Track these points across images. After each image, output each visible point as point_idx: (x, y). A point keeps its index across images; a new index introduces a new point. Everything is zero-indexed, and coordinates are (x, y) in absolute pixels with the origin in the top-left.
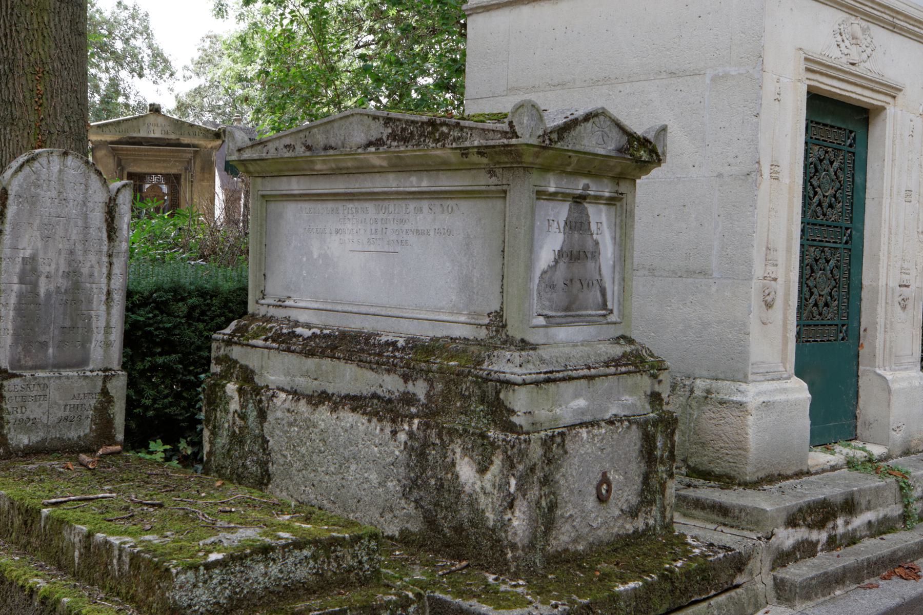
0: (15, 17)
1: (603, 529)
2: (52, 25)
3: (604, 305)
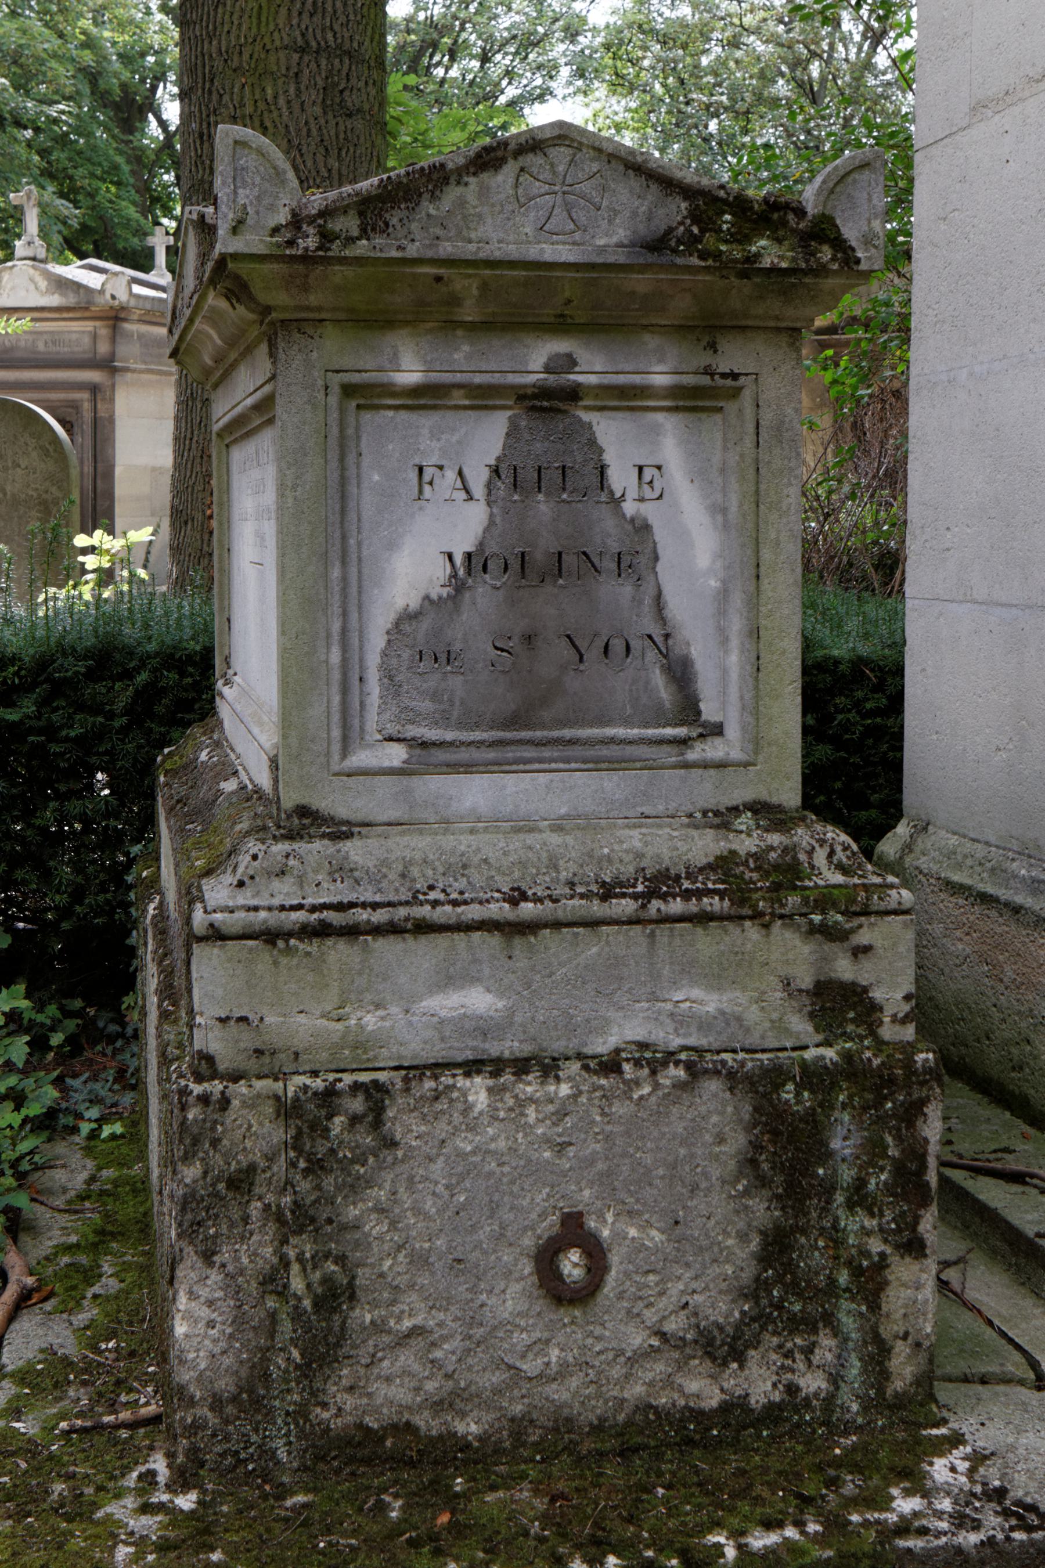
0: (215, 97)
1: (574, 1382)
2: (282, 101)
3: (688, 709)
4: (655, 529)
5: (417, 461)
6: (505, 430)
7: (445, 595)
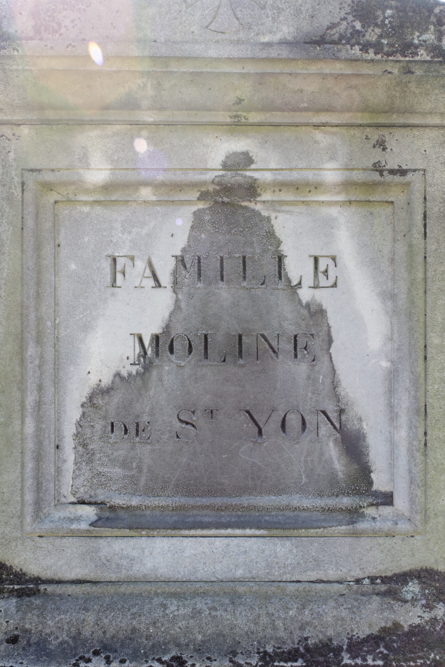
3: (360, 478)
4: (330, 314)
5: (110, 252)
6: (190, 224)
7: (134, 372)
